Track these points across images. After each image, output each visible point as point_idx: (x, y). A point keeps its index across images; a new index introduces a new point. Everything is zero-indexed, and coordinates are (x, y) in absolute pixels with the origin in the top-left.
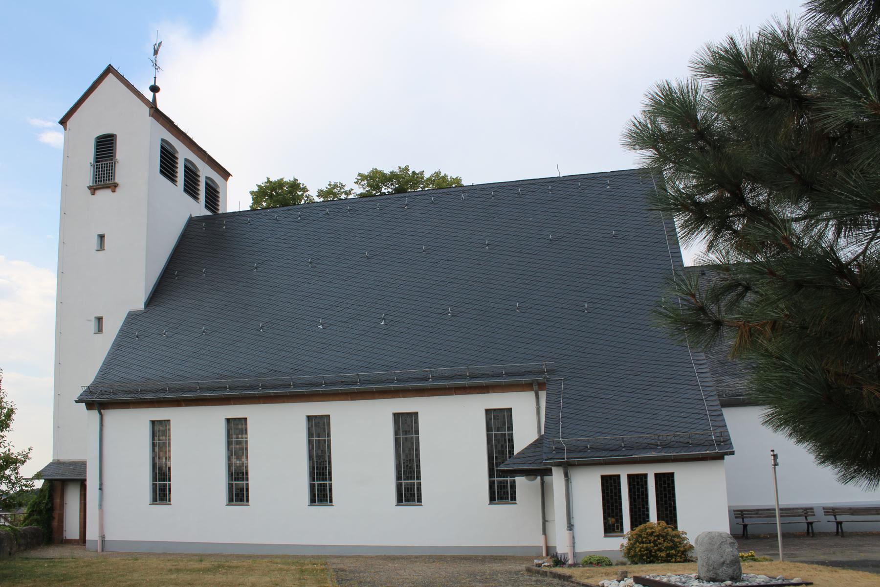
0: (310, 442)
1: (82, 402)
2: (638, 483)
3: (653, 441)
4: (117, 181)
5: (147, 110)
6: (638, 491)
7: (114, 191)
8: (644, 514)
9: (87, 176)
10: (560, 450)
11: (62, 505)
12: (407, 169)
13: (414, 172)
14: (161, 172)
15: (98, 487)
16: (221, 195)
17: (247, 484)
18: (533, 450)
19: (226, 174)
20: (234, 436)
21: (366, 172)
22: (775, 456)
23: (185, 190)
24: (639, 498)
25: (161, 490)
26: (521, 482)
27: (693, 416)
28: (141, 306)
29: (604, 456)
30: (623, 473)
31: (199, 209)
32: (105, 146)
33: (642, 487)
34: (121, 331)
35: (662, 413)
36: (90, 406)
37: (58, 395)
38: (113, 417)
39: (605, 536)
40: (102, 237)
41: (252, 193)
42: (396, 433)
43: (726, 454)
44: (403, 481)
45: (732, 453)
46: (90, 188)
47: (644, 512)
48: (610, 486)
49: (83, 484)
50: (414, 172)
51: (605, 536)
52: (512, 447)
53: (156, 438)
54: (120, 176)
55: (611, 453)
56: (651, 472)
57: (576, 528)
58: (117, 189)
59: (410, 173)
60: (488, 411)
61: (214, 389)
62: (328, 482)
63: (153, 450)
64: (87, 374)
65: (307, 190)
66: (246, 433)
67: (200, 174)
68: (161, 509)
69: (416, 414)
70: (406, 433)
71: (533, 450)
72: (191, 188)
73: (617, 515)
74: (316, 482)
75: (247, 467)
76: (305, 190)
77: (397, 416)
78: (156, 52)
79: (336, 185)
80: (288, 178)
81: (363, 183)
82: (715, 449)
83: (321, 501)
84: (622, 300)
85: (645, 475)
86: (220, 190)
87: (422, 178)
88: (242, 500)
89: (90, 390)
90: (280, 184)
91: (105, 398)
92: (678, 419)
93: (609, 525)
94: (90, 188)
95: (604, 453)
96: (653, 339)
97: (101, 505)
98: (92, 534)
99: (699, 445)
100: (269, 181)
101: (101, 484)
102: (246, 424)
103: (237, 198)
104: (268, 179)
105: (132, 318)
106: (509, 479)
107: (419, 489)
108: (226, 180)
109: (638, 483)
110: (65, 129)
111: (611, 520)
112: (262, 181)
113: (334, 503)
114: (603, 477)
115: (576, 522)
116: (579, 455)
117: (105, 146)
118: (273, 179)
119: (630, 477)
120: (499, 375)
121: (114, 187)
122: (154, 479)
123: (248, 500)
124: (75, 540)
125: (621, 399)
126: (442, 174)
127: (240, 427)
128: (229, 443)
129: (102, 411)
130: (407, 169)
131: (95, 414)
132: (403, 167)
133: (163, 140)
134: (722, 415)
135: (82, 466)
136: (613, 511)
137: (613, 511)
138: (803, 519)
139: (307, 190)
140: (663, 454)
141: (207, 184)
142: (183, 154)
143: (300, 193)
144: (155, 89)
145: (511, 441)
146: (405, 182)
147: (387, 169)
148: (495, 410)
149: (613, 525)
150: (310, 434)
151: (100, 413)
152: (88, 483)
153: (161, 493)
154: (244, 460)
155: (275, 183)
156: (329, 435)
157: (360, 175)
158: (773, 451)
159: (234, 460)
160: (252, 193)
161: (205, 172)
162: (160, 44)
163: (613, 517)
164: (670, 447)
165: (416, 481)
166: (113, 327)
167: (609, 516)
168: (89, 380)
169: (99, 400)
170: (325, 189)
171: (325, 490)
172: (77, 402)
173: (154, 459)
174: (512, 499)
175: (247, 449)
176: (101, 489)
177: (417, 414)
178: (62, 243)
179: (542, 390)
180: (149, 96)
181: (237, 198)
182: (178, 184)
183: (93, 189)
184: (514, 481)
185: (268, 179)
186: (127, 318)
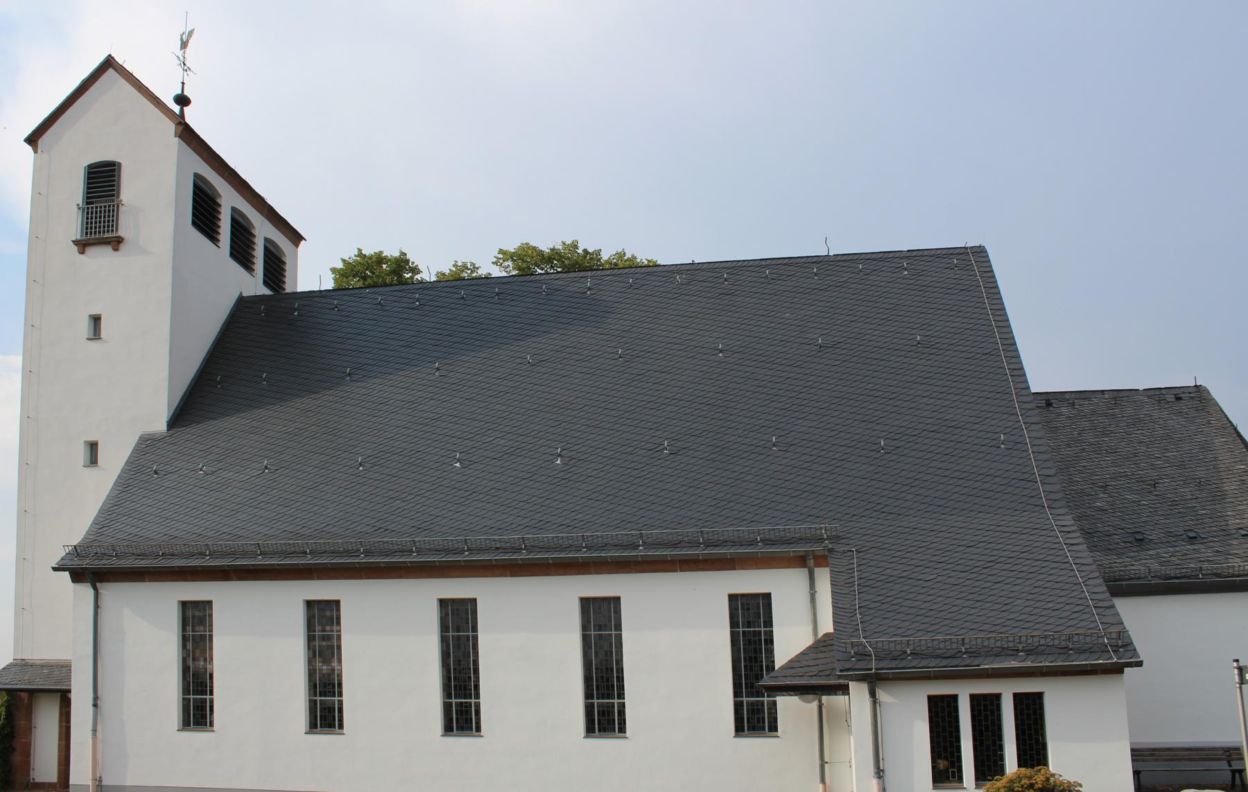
0: (444, 640)
1: (64, 570)
2: (986, 709)
3: (1011, 645)
4: (121, 233)
5: (171, 127)
6: (986, 720)
7: (116, 249)
8: (995, 754)
9: (72, 225)
10: (863, 655)
11: (29, 729)
12: (575, 246)
13: (585, 251)
14: (194, 223)
15: (91, 702)
16: (287, 267)
17: (341, 702)
18: (814, 656)
19: (296, 238)
20: (318, 628)
21: (511, 247)
22: (1240, 669)
23: (232, 255)
24: (987, 729)
25: (196, 708)
26: (787, 705)
27: (1068, 607)
28: (161, 426)
29: (934, 665)
30: (964, 693)
31: (254, 285)
32: (102, 181)
33: (992, 715)
34: (128, 463)
35: (1018, 602)
36: (78, 576)
37: (22, 560)
38: (113, 593)
39: (935, 788)
40: (96, 320)
41: (334, 270)
42: (585, 627)
43: (1130, 665)
44: (595, 701)
45: (1140, 664)
46: (76, 243)
47: (995, 751)
48: (942, 716)
49: (64, 698)
50: (585, 251)
51: (935, 788)
52: (770, 652)
53: (189, 628)
54: (125, 228)
55: (945, 662)
56: (1007, 692)
57: (888, 776)
58: (122, 247)
59: (580, 251)
60: (733, 598)
61: (287, 554)
62: (473, 701)
63: (184, 646)
64: (74, 525)
65: (419, 272)
66: (339, 623)
67: (256, 232)
68: (197, 738)
69: (617, 600)
70: (599, 627)
71: (814, 656)
72: (241, 252)
73: (952, 756)
74: (454, 701)
75: (340, 675)
76: (415, 270)
77: (586, 603)
78: (184, 45)
79: (465, 267)
80: (391, 252)
81: (506, 264)
82: (1110, 659)
83: (604, 730)
84: (938, 436)
85: (997, 697)
86: (287, 259)
87: (599, 260)
88: (331, 726)
89: (76, 551)
90: (380, 259)
91: (105, 563)
92: (1044, 613)
93: (940, 772)
94: (76, 243)
95: (934, 662)
96: (989, 494)
97: (95, 730)
98: (80, 774)
99: (1085, 651)
100: (360, 254)
101: (96, 698)
102: (338, 610)
103: (312, 272)
104: (360, 250)
105: (147, 444)
106: (766, 699)
107: (622, 713)
108: (297, 246)
109: (986, 709)
110: (36, 151)
111: (942, 764)
112: (351, 254)
113: (345, 730)
114: (930, 698)
115: (887, 765)
116: (893, 664)
117: (102, 181)
118: (368, 251)
119: (974, 698)
120: (752, 543)
121: (117, 243)
122: (186, 690)
123: (341, 726)
124: (51, 785)
125: (950, 580)
126: (628, 255)
127: (328, 613)
128: (310, 639)
129: (98, 585)
130: (575, 246)
131: (86, 591)
132: (569, 242)
133: (197, 176)
134: (1113, 606)
135: (64, 669)
136: (946, 751)
137: (946, 751)
138: (1224, 765)
139: (419, 272)
140: (1029, 664)
141: (266, 248)
142: (229, 199)
143: (407, 276)
144: (183, 100)
145: (770, 641)
146: (576, 263)
147: (545, 245)
148: (743, 595)
149: (947, 770)
150: (444, 627)
151: (95, 588)
152: (74, 696)
153: (197, 711)
154: (335, 664)
155: (371, 258)
156: (475, 629)
157: (501, 251)
158: (1237, 661)
159: (318, 665)
160: (334, 270)
161: (262, 230)
162: (191, 33)
163: (946, 758)
164: (1037, 654)
165: (616, 701)
166: (115, 459)
167: (940, 757)
168: (76, 538)
169: (91, 569)
170: (447, 272)
171: (468, 712)
172: (55, 569)
173: (184, 660)
174: (770, 730)
175: (339, 647)
176: (95, 705)
177: (619, 598)
178: (30, 326)
179: (819, 565)
180: (176, 109)
181: (312, 272)
182: (220, 244)
183: (82, 245)
184: (775, 703)
185: (360, 250)
186: (138, 444)
